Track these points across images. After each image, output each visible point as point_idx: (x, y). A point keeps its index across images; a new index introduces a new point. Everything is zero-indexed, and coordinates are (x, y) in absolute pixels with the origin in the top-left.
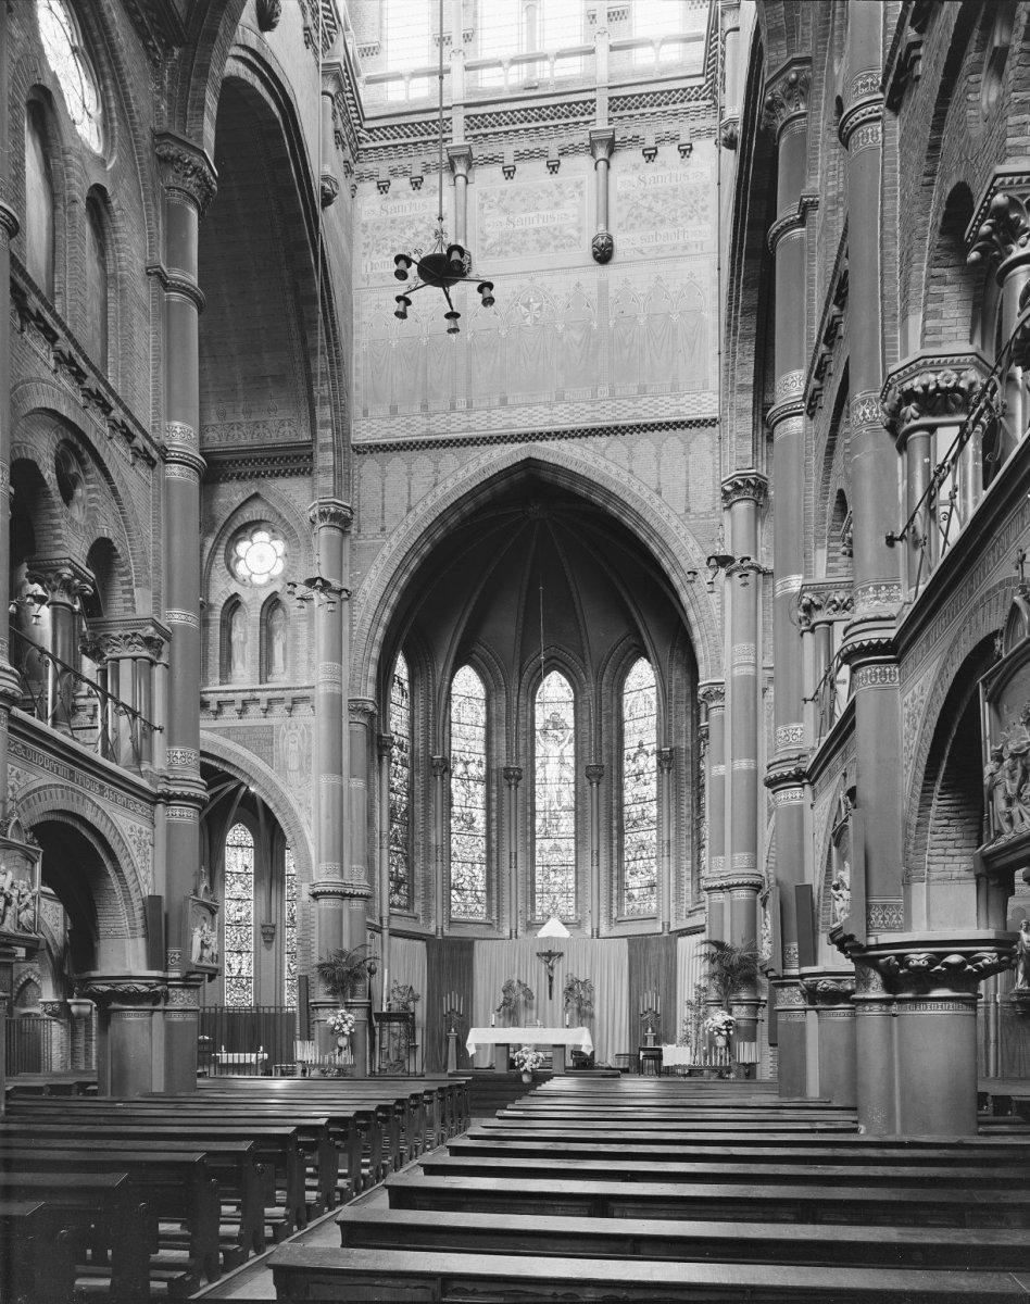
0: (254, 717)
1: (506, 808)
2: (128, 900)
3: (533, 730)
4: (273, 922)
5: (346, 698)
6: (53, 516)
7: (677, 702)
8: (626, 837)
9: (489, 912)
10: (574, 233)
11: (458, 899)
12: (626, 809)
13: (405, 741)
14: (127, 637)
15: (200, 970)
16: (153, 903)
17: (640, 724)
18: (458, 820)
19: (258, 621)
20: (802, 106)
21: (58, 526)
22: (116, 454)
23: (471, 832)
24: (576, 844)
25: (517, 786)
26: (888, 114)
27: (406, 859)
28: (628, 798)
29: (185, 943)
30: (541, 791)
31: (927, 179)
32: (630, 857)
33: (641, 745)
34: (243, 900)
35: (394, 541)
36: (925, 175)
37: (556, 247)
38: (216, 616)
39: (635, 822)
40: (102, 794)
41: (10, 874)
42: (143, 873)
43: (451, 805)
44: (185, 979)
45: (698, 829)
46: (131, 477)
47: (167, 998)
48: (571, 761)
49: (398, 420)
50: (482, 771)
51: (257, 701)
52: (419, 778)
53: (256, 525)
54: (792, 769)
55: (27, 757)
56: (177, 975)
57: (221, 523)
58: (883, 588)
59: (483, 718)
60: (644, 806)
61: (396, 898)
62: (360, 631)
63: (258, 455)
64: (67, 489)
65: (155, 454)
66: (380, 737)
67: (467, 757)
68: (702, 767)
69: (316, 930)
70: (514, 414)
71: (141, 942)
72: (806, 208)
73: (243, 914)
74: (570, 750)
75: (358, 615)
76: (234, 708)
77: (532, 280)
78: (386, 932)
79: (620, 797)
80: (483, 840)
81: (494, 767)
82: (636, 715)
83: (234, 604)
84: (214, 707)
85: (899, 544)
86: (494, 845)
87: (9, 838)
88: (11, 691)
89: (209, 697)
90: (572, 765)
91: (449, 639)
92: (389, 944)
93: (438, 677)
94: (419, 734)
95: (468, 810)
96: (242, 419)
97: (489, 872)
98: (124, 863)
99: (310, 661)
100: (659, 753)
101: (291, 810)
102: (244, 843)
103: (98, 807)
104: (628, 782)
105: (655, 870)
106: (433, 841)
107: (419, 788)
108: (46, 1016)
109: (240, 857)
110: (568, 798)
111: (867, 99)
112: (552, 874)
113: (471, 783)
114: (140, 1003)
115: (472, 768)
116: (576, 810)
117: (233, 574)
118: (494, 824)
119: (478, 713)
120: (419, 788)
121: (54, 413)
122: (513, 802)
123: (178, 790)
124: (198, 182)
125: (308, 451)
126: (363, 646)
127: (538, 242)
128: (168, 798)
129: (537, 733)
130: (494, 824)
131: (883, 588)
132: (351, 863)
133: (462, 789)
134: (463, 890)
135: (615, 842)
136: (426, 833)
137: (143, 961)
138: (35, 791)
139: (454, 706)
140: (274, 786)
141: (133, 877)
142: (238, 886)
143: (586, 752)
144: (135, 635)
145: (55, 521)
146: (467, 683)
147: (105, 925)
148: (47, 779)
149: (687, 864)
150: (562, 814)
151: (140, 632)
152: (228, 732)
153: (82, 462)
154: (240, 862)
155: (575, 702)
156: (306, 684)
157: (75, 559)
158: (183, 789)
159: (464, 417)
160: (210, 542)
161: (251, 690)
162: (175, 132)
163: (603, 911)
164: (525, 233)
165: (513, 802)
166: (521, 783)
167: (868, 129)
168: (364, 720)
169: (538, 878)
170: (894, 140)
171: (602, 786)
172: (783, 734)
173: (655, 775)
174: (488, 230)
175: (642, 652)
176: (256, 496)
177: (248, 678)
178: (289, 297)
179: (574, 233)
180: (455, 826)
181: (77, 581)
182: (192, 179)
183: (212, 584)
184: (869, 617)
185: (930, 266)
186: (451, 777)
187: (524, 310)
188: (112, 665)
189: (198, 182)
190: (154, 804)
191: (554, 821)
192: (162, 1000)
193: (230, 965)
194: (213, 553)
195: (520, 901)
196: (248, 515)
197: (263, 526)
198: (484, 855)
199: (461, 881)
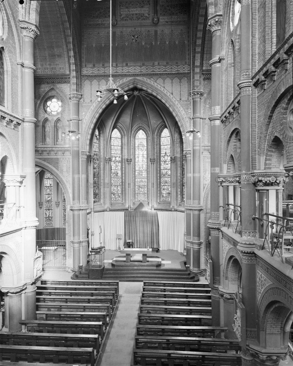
3: (135, 147)
4: (59, 201)
7: (176, 144)
8: (162, 179)
9: (123, 200)
10: (147, 15)
11: (113, 197)
20: (219, 27)
24: (147, 180)
26: (253, 87)
28: (162, 168)
37: (142, 19)
38: (41, 124)
45: (182, 180)
49: (95, 68)
50: (120, 159)
58: (251, 233)
62: (84, 131)
72: (220, 61)
73: (50, 198)
77: (135, 29)
79: (160, 168)
81: (124, 158)
82: (164, 144)
86: (124, 181)
91: (110, 124)
96: (48, 67)
97: (122, 188)
104: (162, 163)
105: (170, 189)
106: (106, 182)
109: (49, 182)
110: (145, 167)
115: (117, 159)
117: (46, 111)
118: (124, 174)
124: (33, 33)
126: (85, 136)
127: (137, 17)
129: (136, 148)
130: (124, 174)
133: (114, 165)
134: (115, 194)
135: (158, 180)
136: (104, 180)
140: (59, 176)
149: (179, 190)
150: (143, 171)
154: (49, 183)
155: (147, 139)
160: (39, 102)
161: (52, 148)
162: (27, 20)
164: (133, 15)
165: (129, 179)
166: (131, 163)
167: (247, 89)
171: (155, 164)
172: (213, 214)
173: (170, 162)
174: (122, 13)
179: (147, 15)
187: (133, 37)
189: (33, 33)
191: (141, 173)
195: (131, 197)
196: (50, 94)
197: (55, 97)
198: (121, 183)
199: (114, 191)
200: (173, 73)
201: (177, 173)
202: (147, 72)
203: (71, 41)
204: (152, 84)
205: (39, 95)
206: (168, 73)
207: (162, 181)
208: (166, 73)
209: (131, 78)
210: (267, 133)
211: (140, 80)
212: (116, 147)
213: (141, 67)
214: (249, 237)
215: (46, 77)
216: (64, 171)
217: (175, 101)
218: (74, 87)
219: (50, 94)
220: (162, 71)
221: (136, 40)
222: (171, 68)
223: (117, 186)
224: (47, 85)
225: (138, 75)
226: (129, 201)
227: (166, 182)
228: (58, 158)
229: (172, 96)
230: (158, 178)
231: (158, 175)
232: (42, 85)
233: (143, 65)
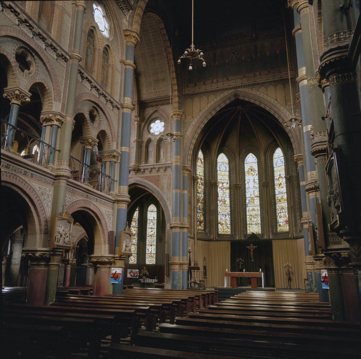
0: (154, 173)
2: (103, 233)
6: (88, 126)
12: (276, 196)
15: (124, 254)
16: (111, 233)
17: (280, 168)
18: (220, 201)
19: (156, 145)
21: (89, 129)
22: (108, 108)
23: (225, 205)
26: (310, 5)
27: (203, 215)
28: (277, 192)
29: (120, 245)
30: (248, 191)
31: (319, 21)
32: (279, 212)
33: (280, 175)
34: (153, 228)
35: (196, 120)
36: (319, 20)
38: (144, 144)
39: (280, 200)
40: (96, 201)
41: (63, 227)
42: (109, 224)
44: (120, 257)
46: (113, 114)
47: (114, 263)
48: (257, 181)
50: (228, 186)
51: (155, 168)
53: (156, 119)
54: (313, 186)
55: (73, 193)
56: (118, 256)
57: (146, 119)
58: (322, 132)
59: (228, 169)
60: (282, 195)
63: (157, 100)
64: (93, 118)
65: (119, 106)
66: (194, 177)
67: (223, 181)
69: (172, 239)
70: (230, 82)
71: (107, 246)
73: (153, 233)
74: (257, 178)
78: (196, 239)
80: (229, 207)
82: (278, 165)
83: (149, 141)
84: (142, 170)
85: (326, 119)
87: (63, 217)
88: (68, 175)
90: (258, 182)
91: (215, 147)
92: (197, 243)
93: (213, 157)
95: (224, 198)
96: (153, 91)
98: (102, 221)
99: (171, 156)
100: (286, 177)
101: (165, 201)
102: (154, 210)
103: (95, 205)
108: (89, 266)
109: (152, 215)
110: (257, 193)
111: (303, 3)
112: (253, 218)
113: (225, 189)
114: (106, 265)
115: (225, 185)
116: (260, 197)
117: (149, 132)
119: (226, 168)
121: (90, 100)
123: (121, 199)
128: (118, 201)
131: (322, 132)
133: (221, 191)
134: (223, 224)
137: (107, 251)
138: (75, 202)
139: (218, 166)
140: (160, 194)
141: (105, 225)
142: (151, 224)
144: (110, 155)
145: (88, 127)
147: (96, 240)
148: (80, 198)
150: (255, 198)
151: (112, 154)
152: (146, 178)
153: (97, 111)
154: (152, 216)
155: (258, 162)
156: (169, 162)
157: (93, 137)
158: (122, 198)
160: (143, 124)
161: (154, 165)
162: (130, 29)
167: (305, 9)
170: (312, 11)
175: (277, 146)
176: (156, 111)
177: (152, 162)
178: (166, 59)
181: (93, 143)
182: (133, 39)
184: (318, 141)
185: (324, 43)
186: (217, 188)
188: (104, 164)
190: (114, 203)
192: (113, 264)
193: (148, 249)
195: (242, 227)
198: (229, 213)
199: (222, 221)
200: (275, 80)
202: (248, 83)
203: (171, 51)
204: (254, 93)
205: (144, 117)
206: (271, 81)
207: (277, 208)
208: (269, 81)
209: (232, 91)
210: (321, 32)
211: (242, 91)
212: (223, 172)
213: (241, 79)
214: (320, 137)
215: (151, 101)
216: (165, 187)
217: (280, 106)
218: (176, 105)
219: (154, 116)
220: (264, 79)
221: (236, 57)
222: (274, 76)
223: (226, 215)
224: (151, 109)
225: (239, 87)
226: (240, 233)
227: (283, 208)
228: (159, 176)
229: (276, 102)
232: (147, 109)
233: (244, 77)
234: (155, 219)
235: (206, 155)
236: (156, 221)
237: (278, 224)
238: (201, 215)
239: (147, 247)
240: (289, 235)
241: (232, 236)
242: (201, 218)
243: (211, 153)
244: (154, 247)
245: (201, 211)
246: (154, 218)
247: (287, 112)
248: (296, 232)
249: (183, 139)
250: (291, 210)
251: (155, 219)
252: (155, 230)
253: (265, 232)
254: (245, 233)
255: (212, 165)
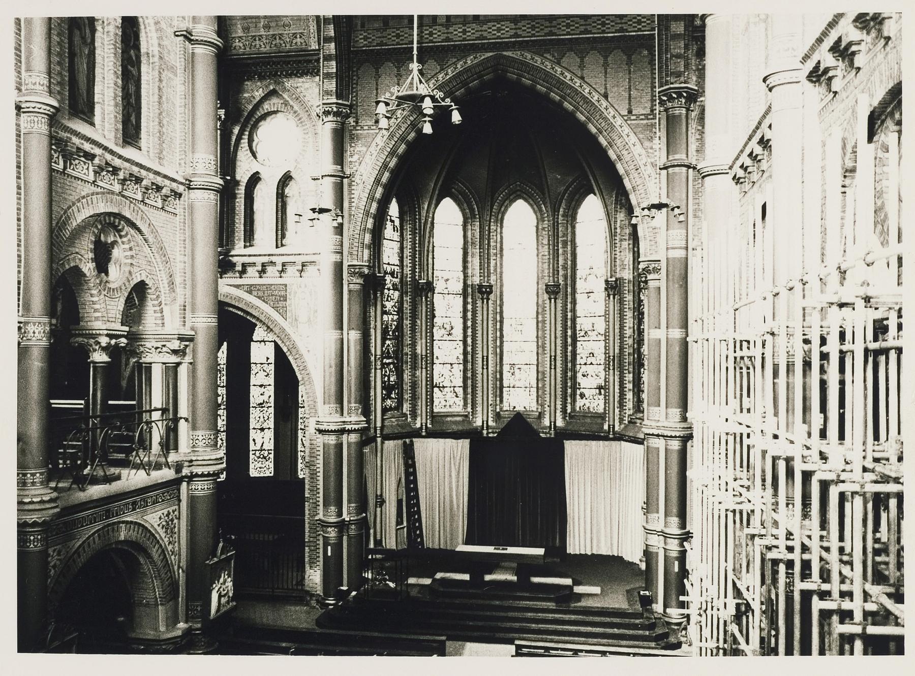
1: (479, 318)
5: (345, 264)
7: (621, 240)
9: (465, 405)
13: (396, 268)
14: (157, 348)
23: (450, 338)
25: (488, 299)
38: (241, 191)
43: (434, 316)
51: (273, 263)
52: (407, 299)
61: (389, 402)
68: (642, 298)
69: (321, 458)
70: (485, 27)
75: (356, 194)
76: (256, 268)
81: (469, 282)
83: (255, 179)
84: (239, 268)
86: (469, 349)
89: (234, 259)
94: (407, 262)
106: (419, 351)
107: (407, 306)
120: (407, 306)
122: (485, 313)
125: (316, 57)
132: (349, 402)
134: (444, 387)
135: (570, 348)
136: (413, 345)
143: (546, 271)
146: (447, 216)
152: (250, 289)
159: (444, 30)
163: (559, 407)
165: (485, 313)
166: (492, 297)
168: (360, 281)
169: (506, 375)
171: (559, 302)
180: (438, 333)
183: (238, 163)
193: (254, 440)
194: (239, 138)
195: (490, 396)
201: (622, 328)
219: (267, 107)
223: (451, 364)
224: (259, 83)
229: (604, 103)
230: (569, 340)
231: (569, 333)
234: (269, 361)
235: (406, 208)
236: (272, 367)
237: (578, 392)
238: (390, 370)
239: (253, 434)
240: (603, 425)
241: (466, 416)
242: (392, 379)
243: (419, 202)
244: (270, 434)
245: (390, 361)
246: (268, 359)
247: (632, 135)
248: (621, 420)
249: (350, 185)
250: (614, 365)
251: (269, 361)
252: (270, 391)
253: (547, 409)
254: (498, 410)
255: (420, 233)
